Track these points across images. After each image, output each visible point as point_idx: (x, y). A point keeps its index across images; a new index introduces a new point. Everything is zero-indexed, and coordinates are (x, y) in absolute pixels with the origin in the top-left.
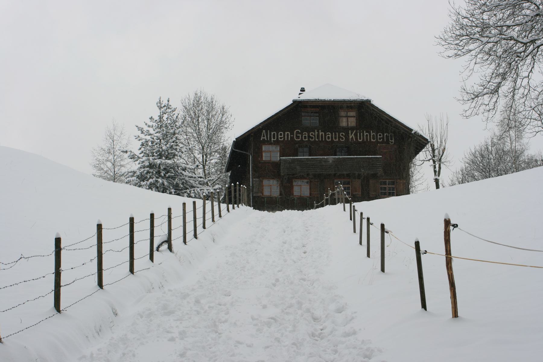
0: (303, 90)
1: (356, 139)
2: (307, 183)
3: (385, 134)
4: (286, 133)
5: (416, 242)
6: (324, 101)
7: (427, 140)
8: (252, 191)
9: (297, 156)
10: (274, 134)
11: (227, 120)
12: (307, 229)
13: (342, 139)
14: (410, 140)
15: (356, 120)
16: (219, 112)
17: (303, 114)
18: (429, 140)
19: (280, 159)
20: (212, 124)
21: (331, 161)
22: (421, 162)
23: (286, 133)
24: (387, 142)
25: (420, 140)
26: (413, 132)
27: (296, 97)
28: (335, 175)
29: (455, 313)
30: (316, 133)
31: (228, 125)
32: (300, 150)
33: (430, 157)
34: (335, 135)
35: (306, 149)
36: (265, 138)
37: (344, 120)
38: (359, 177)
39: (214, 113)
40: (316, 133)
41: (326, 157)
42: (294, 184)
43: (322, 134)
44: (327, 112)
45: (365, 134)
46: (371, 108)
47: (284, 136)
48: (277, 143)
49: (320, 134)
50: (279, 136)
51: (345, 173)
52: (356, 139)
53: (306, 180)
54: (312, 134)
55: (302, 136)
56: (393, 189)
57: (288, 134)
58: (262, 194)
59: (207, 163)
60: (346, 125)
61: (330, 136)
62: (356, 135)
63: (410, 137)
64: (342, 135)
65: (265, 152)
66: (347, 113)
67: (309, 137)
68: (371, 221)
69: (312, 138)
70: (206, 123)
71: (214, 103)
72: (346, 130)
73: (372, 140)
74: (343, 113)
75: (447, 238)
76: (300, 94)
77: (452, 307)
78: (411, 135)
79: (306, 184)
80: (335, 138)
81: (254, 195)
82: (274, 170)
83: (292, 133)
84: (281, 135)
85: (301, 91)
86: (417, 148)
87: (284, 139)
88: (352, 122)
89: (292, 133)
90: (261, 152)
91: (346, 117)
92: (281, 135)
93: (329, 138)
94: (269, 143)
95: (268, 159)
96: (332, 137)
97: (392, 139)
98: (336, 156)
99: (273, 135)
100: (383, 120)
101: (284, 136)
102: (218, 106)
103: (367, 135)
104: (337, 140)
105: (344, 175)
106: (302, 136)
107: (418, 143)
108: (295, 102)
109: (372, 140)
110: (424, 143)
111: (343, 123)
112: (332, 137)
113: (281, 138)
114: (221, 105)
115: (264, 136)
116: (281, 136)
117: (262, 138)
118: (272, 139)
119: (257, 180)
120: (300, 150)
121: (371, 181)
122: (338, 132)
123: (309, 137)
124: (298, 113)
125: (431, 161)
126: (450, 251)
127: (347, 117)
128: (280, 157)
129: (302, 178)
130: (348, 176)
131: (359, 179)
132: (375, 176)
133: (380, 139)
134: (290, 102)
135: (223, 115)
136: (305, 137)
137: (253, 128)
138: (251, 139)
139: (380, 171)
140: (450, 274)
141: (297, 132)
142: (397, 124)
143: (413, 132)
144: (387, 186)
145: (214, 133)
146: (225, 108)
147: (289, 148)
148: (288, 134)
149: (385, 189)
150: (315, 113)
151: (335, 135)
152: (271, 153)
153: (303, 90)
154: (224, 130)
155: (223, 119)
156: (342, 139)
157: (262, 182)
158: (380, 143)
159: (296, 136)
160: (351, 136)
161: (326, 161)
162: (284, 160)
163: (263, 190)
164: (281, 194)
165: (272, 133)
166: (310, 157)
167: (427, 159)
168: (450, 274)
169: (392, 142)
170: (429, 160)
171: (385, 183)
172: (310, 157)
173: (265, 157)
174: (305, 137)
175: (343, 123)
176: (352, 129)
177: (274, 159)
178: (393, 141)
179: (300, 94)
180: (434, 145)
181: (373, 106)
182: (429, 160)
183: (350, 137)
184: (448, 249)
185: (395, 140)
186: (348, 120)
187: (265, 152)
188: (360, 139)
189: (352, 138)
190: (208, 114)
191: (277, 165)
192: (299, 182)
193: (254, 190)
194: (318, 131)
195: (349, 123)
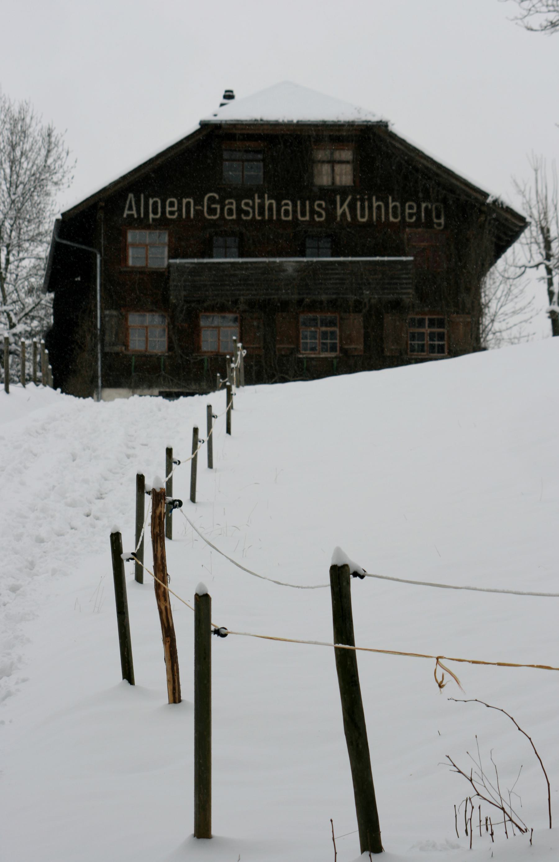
0: (229, 96)
1: (354, 216)
2: (235, 320)
3: (423, 205)
4: (185, 201)
5: (112, 535)
6: (276, 125)
7: (522, 219)
8: (103, 341)
9: (211, 256)
10: (155, 203)
11: (59, 162)
12: (130, 452)
13: (320, 215)
14: (482, 218)
15: (354, 170)
16: (40, 143)
17: (226, 155)
18: (528, 219)
19: (169, 266)
20: (22, 172)
21: (290, 270)
22: (519, 271)
23: (185, 201)
24: (429, 224)
25: (506, 219)
26: (490, 200)
27: (208, 115)
28: (300, 302)
29: (174, 694)
30: (257, 201)
31: (59, 175)
32: (219, 241)
33: (538, 258)
34: (303, 206)
35: (231, 241)
36: (134, 212)
37: (326, 168)
38: (358, 306)
39: (27, 146)
40: (257, 201)
41: (278, 260)
42: (202, 323)
43: (271, 205)
44: (280, 151)
45: (375, 205)
46: (388, 140)
47: (180, 209)
48: (162, 223)
49: (267, 203)
50: (168, 209)
51: (324, 297)
52: (354, 216)
53: (231, 316)
54: (247, 204)
55: (222, 209)
56: (441, 337)
57: (188, 204)
58: (126, 345)
59: (11, 267)
60: (330, 183)
61: (290, 208)
62: (352, 207)
63: (481, 212)
64: (320, 206)
65: (134, 245)
66: (332, 154)
67: (240, 211)
68: (175, 456)
69: (247, 213)
70: (8, 171)
71: (28, 120)
72: (330, 194)
73: (392, 219)
74: (321, 155)
75: (157, 530)
76: (222, 105)
77: (168, 681)
78: (484, 209)
79: (231, 324)
80: (303, 214)
81: (107, 349)
82: (152, 290)
83: (199, 201)
84: (172, 204)
85: (225, 97)
86: (499, 238)
87: (180, 215)
88: (345, 176)
89: (199, 201)
90: (124, 250)
91: (328, 162)
92: (172, 204)
93: (287, 213)
94: (141, 223)
95: (140, 264)
96: (295, 212)
97: (438, 217)
98: (304, 256)
99: (154, 206)
100: (417, 170)
101: (180, 209)
102: (36, 130)
103: (379, 207)
104: (307, 218)
105: (321, 302)
106: (222, 209)
107: (505, 227)
108: (205, 126)
109: (392, 219)
110: (516, 226)
111: (323, 177)
112: (295, 212)
113: (172, 213)
114: (45, 124)
115: (130, 208)
116: (172, 208)
117: (126, 213)
118: (151, 216)
119: (115, 313)
120: (219, 241)
121: (388, 319)
122: (309, 199)
123: (240, 211)
124: (209, 152)
125: (542, 268)
126: (163, 558)
127: (333, 162)
128: (170, 257)
129: (223, 309)
130: (333, 305)
131: (360, 311)
132: (396, 306)
133: (411, 215)
134: (192, 126)
135: (49, 151)
136: (230, 212)
137: (104, 190)
138: (101, 215)
139: (408, 296)
140: (163, 608)
141: (212, 200)
142: (454, 181)
143: (490, 200)
144: (427, 330)
145: (27, 195)
146: (54, 134)
147: (190, 238)
148: (188, 204)
149: (421, 336)
150: (247, 151)
151: (303, 206)
152: (148, 251)
153: (229, 96)
154: (50, 188)
155: (50, 161)
156: (320, 215)
157: (126, 320)
158: (410, 225)
159: (209, 208)
160: (342, 209)
161: (280, 268)
162: (178, 266)
163: (127, 336)
164: (170, 348)
165: (151, 201)
166: (240, 260)
167: (533, 263)
168: (163, 608)
169: (439, 225)
170: (537, 266)
171: (421, 323)
172: (240, 260)
173: (134, 258)
174: (230, 212)
175: (323, 177)
176: (344, 191)
177: (153, 265)
178: (442, 221)
179: (222, 105)
180: (548, 231)
181: (393, 136)
182: (537, 266)
183: (339, 212)
184: (159, 555)
185: (447, 217)
186: (336, 171)
187: (134, 245)
188: (363, 216)
189: (344, 214)
190: (13, 148)
191: (159, 279)
192: (216, 320)
193: (107, 338)
194: (261, 197)
195: (338, 179)
